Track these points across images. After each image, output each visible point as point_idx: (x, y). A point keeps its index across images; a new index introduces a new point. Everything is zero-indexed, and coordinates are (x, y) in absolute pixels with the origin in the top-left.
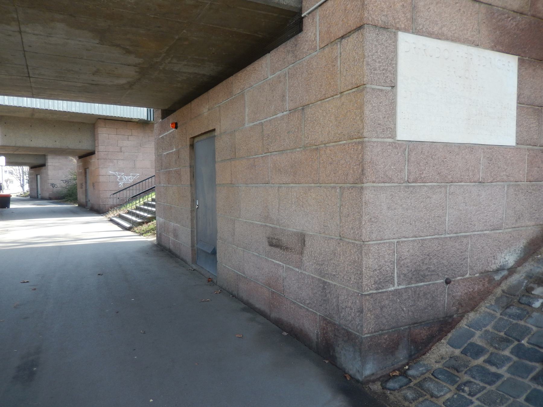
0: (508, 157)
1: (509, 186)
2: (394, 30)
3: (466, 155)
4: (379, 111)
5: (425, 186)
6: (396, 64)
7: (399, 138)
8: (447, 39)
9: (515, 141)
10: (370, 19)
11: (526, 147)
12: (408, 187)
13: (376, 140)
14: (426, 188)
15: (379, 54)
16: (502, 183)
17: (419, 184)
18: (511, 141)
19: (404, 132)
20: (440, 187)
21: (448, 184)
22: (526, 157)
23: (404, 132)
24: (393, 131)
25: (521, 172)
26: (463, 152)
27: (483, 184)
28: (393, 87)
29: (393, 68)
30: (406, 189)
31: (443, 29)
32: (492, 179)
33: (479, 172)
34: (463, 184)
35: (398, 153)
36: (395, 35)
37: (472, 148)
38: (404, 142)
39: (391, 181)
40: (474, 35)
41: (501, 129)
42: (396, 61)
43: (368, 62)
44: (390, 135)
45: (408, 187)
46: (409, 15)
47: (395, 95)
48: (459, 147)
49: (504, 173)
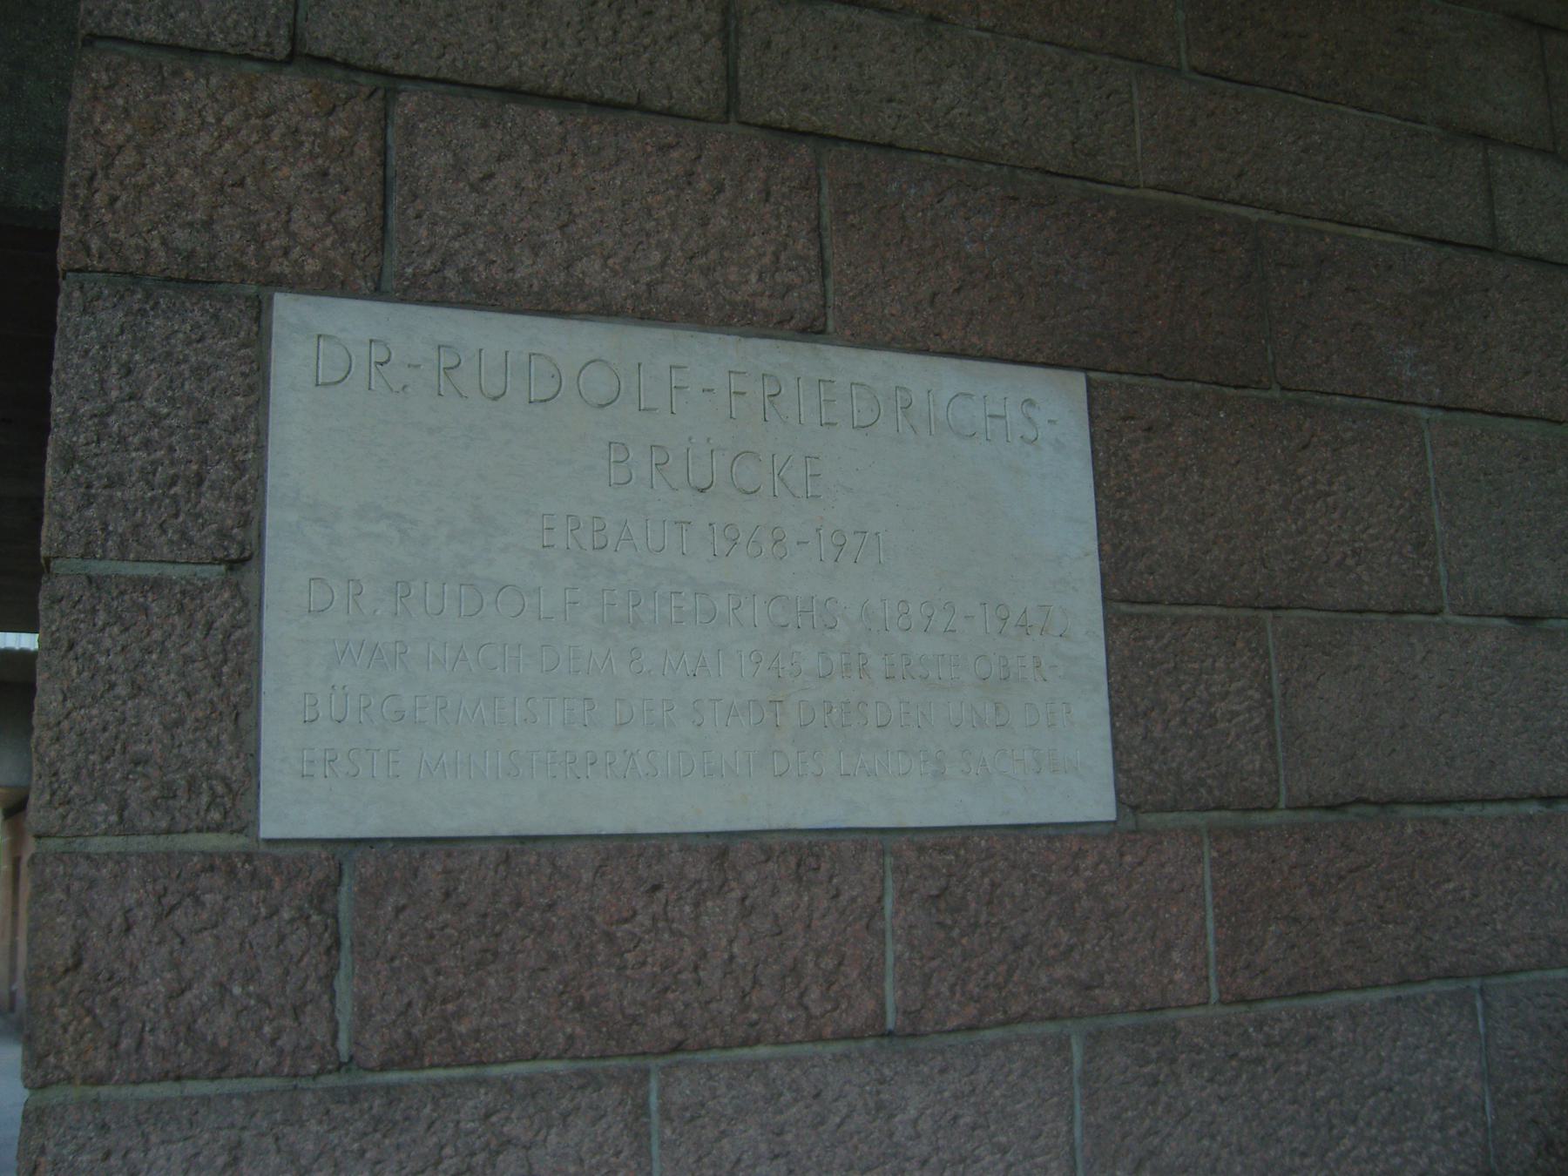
0: (1078, 884)
1: (1094, 1039)
2: (251, 289)
3: (775, 891)
4: (137, 690)
5: (481, 1082)
6: (260, 447)
7: (269, 828)
8: (606, 311)
9: (1110, 796)
10: (95, 243)
11: (1199, 819)
12: (354, 1095)
13: (116, 843)
14: (484, 1097)
15: (149, 403)
16: (1051, 1028)
17: (441, 1074)
18: (1084, 792)
19: (308, 790)
20: (590, 1081)
21: (654, 1063)
22: (1206, 873)
23: (308, 790)
24: (236, 794)
25: (1176, 956)
26: (751, 876)
27: (911, 1043)
28: (234, 565)
29: (240, 468)
30: (337, 1110)
31: (579, 267)
32: (972, 1010)
33: (872, 976)
34: (762, 1051)
35: (274, 912)
36: (260, 312)
37: (806, 853)
38: (315, 850)
39: (223, 1064)
40: (789, 288)
41: (1034, 748)
42: (262, 433)
43: (72, 448)
44: (216, 816)
45: (354, 1095)
46: (354, 216)
47: (250, 607)
48: (685, 849)
49: (1060, 971)
